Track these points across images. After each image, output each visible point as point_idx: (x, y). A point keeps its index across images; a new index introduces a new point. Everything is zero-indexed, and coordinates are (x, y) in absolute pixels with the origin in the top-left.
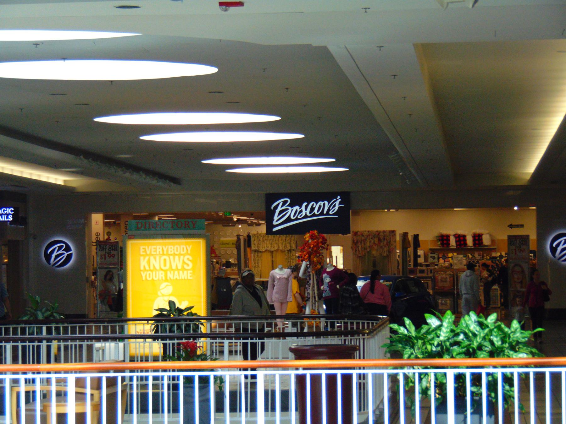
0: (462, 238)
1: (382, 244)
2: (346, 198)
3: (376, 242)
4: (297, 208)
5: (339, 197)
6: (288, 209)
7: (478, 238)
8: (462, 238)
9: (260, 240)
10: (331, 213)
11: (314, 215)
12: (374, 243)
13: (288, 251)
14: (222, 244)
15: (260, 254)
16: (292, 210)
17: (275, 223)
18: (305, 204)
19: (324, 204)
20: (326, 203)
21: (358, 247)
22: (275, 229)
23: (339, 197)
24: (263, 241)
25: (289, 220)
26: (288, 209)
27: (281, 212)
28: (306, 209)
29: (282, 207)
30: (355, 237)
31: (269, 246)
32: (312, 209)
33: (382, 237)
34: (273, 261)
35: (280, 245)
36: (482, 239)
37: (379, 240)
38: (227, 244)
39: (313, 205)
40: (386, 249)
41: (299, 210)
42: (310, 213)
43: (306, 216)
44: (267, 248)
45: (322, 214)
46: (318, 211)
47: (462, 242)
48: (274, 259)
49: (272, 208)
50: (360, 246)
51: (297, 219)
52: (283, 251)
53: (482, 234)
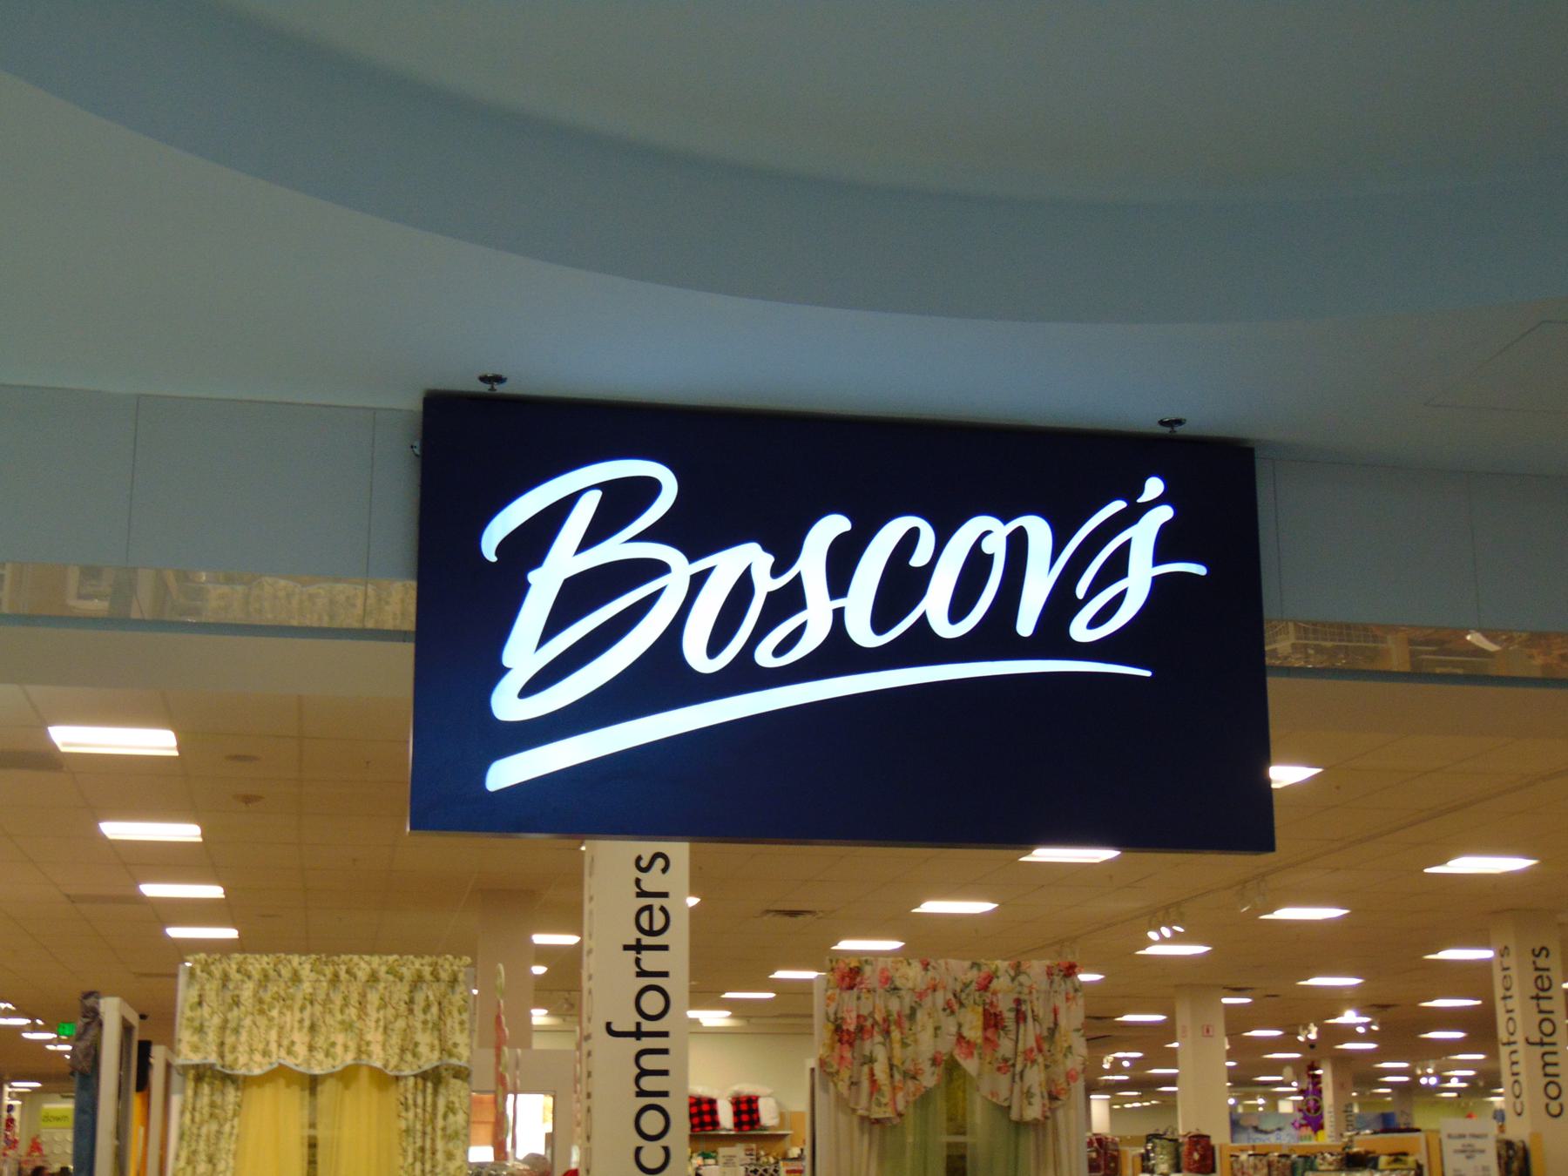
0: (705, 1107)
1: (1005, 1046)
2: (1217, 487)
3: (974, 1033)
4: (751, 557)
5: (1154, 487)
6: (660, 568)
7: (746, 1109)
8: (705, 1107)
9: (236, 1002)
10: (1080, 630)
11: (922, 646)
12: (960, 1038)
13: (424, 1076)
14: (47, 1118)
15: (231, 1095)
16: (698, 582)
17: (507, 704)
18: (833, 526)
19: (1018, 543)
20: (1038, 530)
21: (871, 1060)
22: (505, 773)
23: (1154, 487)
24: (261, 1008)
25: (661, 680)
26: (660, 568)
27: (579, 595)
28: (839, 582)
29: (591, 539)
30: (849, 998)
31: (300, 1038)
32: (903, 584)
33: (1005, 1005)
34: (313, 1145)
35: (374, 1036)
36: (756, 1111)
37: (992, 1021)
38: (58, 1119)
39: (910, 540)
40: (1035, 1077)
41: (765, 584)
42: (882, 619)
43: (838, 654)
44: (279, 1057)
45: (996, 636)
46: (958, 611)
47: (707, 1118)
48: (321, 1133)
49: (489, 546)
50: (881, 1054)
51: (743, 676)
52: (385, 1080)
53: (757, 1098)
